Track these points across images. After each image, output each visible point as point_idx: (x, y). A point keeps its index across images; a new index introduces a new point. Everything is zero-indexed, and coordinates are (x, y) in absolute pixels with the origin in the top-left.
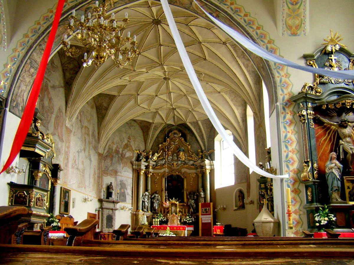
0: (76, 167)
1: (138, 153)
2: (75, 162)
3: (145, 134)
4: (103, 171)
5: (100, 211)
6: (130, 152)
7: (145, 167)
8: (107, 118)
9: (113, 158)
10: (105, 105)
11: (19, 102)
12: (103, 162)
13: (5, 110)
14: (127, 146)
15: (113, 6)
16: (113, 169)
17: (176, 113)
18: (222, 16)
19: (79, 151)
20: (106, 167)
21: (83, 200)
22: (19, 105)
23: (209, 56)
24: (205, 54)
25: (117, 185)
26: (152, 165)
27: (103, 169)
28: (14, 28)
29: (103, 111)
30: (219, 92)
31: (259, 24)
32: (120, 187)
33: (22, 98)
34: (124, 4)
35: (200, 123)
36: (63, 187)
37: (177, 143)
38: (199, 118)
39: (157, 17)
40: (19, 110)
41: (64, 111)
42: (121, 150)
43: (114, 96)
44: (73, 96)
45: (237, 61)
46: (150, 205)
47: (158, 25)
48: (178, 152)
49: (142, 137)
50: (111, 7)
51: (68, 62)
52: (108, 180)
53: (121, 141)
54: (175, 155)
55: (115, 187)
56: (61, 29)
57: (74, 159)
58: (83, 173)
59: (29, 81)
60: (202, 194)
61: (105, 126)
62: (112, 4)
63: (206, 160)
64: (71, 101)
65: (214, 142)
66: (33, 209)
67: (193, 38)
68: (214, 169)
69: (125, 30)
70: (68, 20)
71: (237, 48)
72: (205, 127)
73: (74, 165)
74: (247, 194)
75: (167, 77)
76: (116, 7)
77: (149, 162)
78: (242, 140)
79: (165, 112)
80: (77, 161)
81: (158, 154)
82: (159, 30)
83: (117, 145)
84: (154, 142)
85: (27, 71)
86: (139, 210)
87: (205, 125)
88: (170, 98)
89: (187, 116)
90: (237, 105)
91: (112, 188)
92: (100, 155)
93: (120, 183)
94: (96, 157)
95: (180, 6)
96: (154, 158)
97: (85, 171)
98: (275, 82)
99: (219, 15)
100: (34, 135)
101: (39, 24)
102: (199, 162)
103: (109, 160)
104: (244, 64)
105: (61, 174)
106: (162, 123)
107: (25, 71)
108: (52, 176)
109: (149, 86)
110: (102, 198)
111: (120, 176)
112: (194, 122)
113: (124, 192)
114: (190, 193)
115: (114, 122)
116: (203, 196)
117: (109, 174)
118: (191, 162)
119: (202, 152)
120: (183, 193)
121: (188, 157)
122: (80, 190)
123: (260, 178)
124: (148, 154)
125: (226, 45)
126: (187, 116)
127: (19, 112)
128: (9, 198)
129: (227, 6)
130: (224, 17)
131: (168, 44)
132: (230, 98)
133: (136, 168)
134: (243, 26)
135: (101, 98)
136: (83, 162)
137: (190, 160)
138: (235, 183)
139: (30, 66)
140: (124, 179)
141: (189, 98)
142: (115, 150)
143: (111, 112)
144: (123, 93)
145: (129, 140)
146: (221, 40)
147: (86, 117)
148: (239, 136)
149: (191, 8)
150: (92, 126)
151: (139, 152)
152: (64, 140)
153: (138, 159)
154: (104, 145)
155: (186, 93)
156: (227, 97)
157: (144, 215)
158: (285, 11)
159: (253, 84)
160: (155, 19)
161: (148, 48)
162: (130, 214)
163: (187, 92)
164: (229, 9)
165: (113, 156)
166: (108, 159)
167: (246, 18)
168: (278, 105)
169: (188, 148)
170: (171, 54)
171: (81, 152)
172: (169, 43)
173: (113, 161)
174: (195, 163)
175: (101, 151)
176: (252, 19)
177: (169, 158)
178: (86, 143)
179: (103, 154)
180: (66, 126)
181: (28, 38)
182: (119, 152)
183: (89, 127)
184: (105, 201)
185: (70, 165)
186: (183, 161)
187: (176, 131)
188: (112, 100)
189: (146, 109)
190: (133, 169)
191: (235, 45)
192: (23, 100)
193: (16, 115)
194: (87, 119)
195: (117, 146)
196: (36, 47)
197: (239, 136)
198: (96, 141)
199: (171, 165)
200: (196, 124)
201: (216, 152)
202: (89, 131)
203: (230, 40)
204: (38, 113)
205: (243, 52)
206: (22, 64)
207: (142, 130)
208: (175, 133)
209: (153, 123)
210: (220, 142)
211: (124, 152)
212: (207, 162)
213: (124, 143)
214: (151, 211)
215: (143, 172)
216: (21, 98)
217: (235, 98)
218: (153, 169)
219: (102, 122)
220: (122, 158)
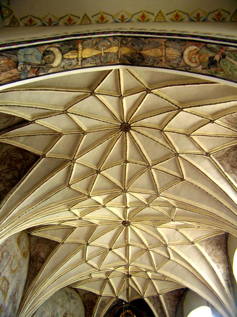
3: (88, 313)
10: (42, 255)
15: (80, 63)
17: (131, 283)
23: (187, 175)
29: (38, 264)
34: (94, 65)
35: (161, 297)
38: (160, 291)
39: (126, 120)
43: (57, 243)
47: (126, 133)
50: (78, 63)
51: (7, 170)
61: (36, 287)
62: (80, 60)
69: (86, 134)
72: (169, 305)
75: (127, 220)
76: (83, 66)
79: (118, 280)
88: (127, 254)
89: (144, 288)
90: (217, 261)
95: (166, 66)
106: (112, 297)
109: (103, 233)
115: (49, 281)
131: (136, 161)
135: (40, 244)
141: (151, 253)
143: (48, 266)
144: (68, 240)
147: (10, 262)
149: (182, 64)
155: (148, 247)
156: (202, 249)
161: (111, 165)
163: (149, 245)
183: (10, 281)
187: (130, 311)
188: (53, 249)
189: (94, 269)
194: (11, 266)
198: (15, 310)
200: (156, 299)
202: (8, 288)
207: (85, 307)
209: (101, 296)
217: (213, 251)
219: (32, 280)
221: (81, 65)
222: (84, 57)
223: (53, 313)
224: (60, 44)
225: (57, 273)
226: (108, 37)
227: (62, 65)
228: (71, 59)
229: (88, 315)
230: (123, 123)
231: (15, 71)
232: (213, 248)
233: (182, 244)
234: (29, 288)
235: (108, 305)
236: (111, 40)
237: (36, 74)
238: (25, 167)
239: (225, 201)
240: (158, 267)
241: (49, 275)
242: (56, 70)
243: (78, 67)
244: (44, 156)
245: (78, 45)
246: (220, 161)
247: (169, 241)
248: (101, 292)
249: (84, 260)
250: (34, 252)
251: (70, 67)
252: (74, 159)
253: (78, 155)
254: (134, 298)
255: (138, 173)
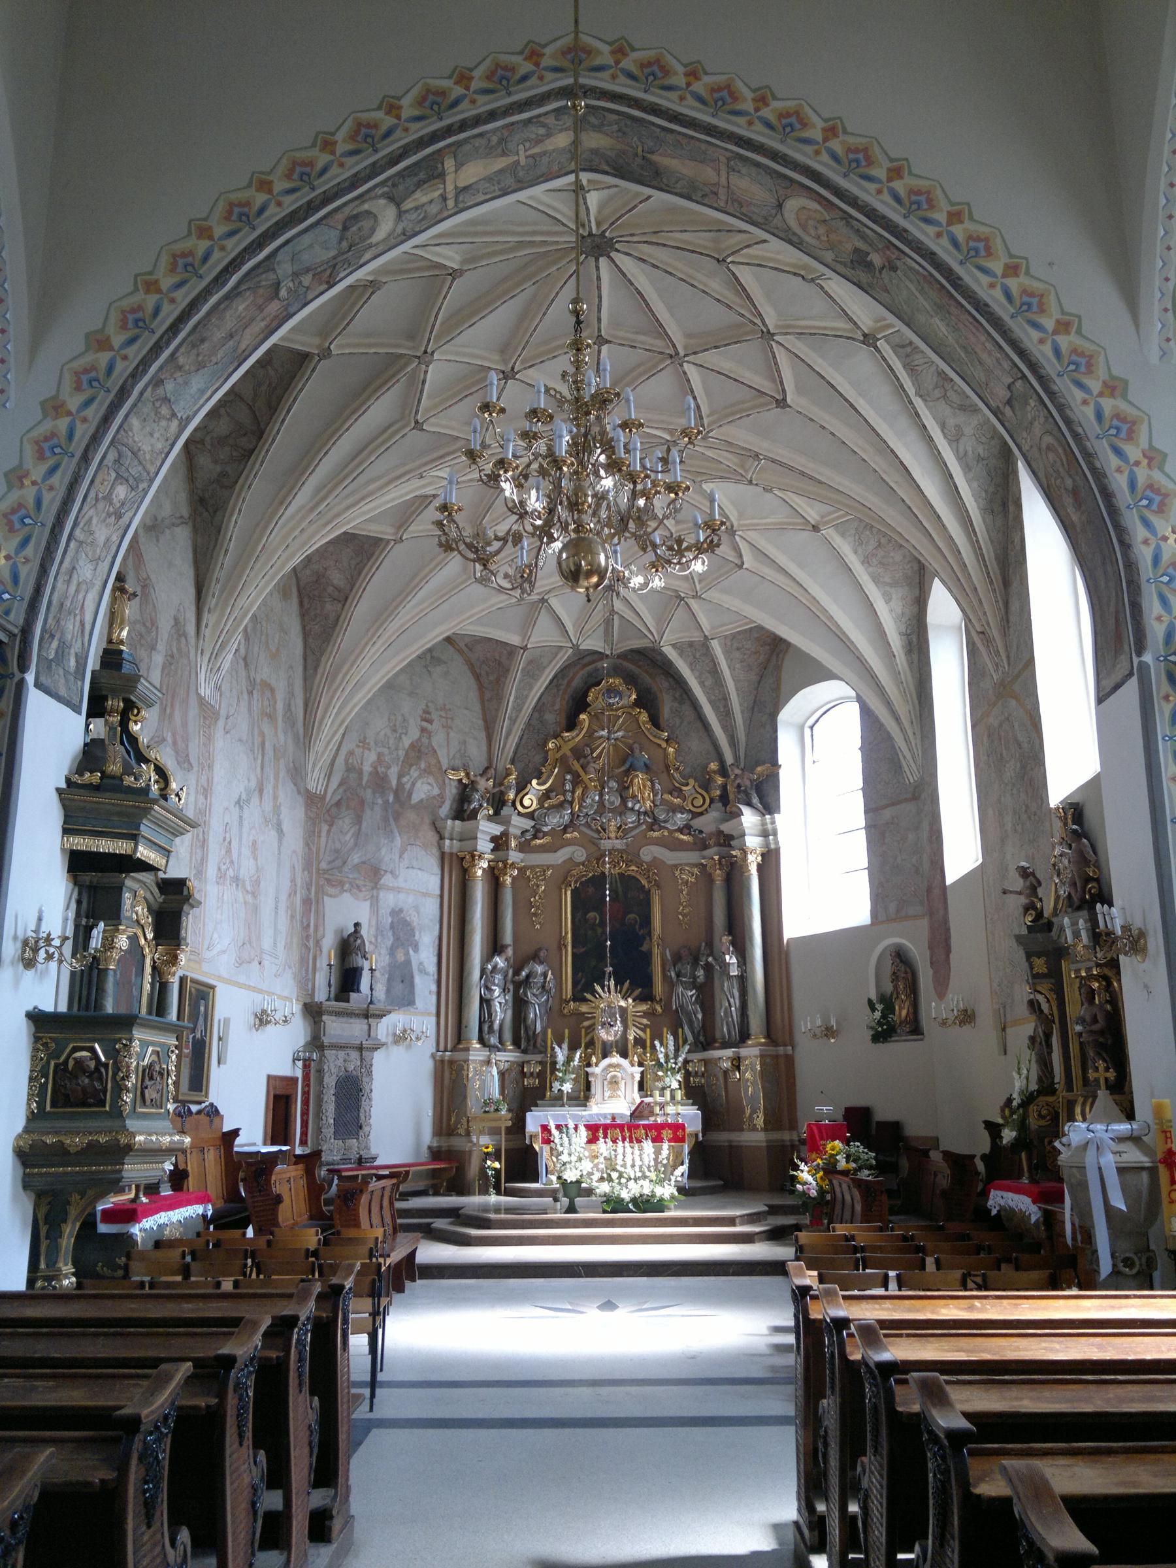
0: (231, 873)
1: (460, 781)
2: (229, 851)
4: (326, 871)
5: (310, 1059)
6: (431, 780)
7: (492, 845)
8: (346, 638)
9: (363, 811)
10: (337, 578)
11: (69, 637)
12: (324, 834)
13: (21, 684)
14: (417, 753)
15: (451, 203)
16: (364, 859)
17: (618, 605)
18: (911, 269)
19: (244, 797)
20: (337, 851)
21: (252, 1019)
22: (67, 650)
23: (799, 390)
24: (782, 383)
25: (379, 931)
26: (518, 832)
27: (324, 865)
28: (47, 305)
29: (328, 607)
30: (815, 528)
31: (1067, 309)
32: (389, 943)
33: (78, 618)
35: (716, 647)
36: (190, 975)
37: (620, 734)
38: (713, 628)
39: (598, 224)
40: (66, 672)
41: (191, 629)
42: (393, 772)
44: (226, 560)
45: (918, 415)
46: (509, 1013)
47: (597, 260)
48: (627, 772)
49: (477, 708)
52: (346, 910)
53: (395, 731)
54: (613, 784)
55: (371, 942)
56: (241, 308)
57: (225, 839)
58: (254, 895)
59: (107, 540)
60: (731, 959)
62: (451, 195)
63: (746, 810)
64: (218, 580)
65: (776, 731)
66: (131, 1124)
67: (743, 316)
68: (777, 850)
70: (274, 270)
71: (918, 360)
73: (223, 868)
74: (931, 972)
77: (506, 822)
78: (903, 730)
80: (234, 844)
81: (545, 783)
82: (599, 279)
83: (379, 750)
84: (523, 731)
85: (104, 498)
86: (469, 1040)
87: (737, 654)
89: (663, 620)
90: (887, 579)
91: (359, 948)
92: (312, 800)
93: (390, 920)
94: (300, 813)
96: (526, 802)
97: (262, 883)
98: (1131, 566)
99: (898, 263)
100: (129, 780)
101: (151, 286)
102: (708, 823)
103: (347, 820)
104: (943, 427)
105: (191, 925)
107: (97, 500)
108: (155, 938)
110: (321, 995)
111: (392, 889)
112: (691, 644)
113: (408, 963)
114: (677, 958)
115: (373, 652)
116: (734, 972)
117: (347, 886)
118: (680, 818)
119: (723, 772)
120: (648, 956)
121: (667, 797)
122: (242, 979)
123: (1024, 931)
124: (501, 784)
125: (876, 348)
126: (663, 620)
127: (67, 680)
128: (31, 1079)
129: (937, 229)
130: (918, 272)
131: (630, 336)
132: (860, 550)
133: (455, 851)
134: (1000, 319)
136: (254, 843)
137: (674, 809)
138: (874, 913)
139: (114, 475)
140: (405, 901)
142: (371, 774)
143: (362, 609)
145: (425, 724)
146: (855, 324)
148: (888, 704)
149: (778, 221)
150: (284, 678)
151: (468, 775)
152: (192, 761)
153: (463, 811)
154: (327, 757)
156: (845, 547)
157: (488, 1062)
158: (1172, 252)
159: (977, 511)
160: (590, 234)
162: (429, 1065)
164: (945, 241)
165: (362, 802)
166: (342, 813)
167: (1013, 284)
168: (1148, 666)
169: (666, 755)
170: (641, 374)
171: (248, 801)
172: (637, 333)
173: (364, 824)
174: (697, 823)
175: (315, 783)
176: (983, 230)
177: (588, 801)
178: (266, 759)
179: (323, 797)
180: (198, 694)
181: (110, 354)
182: (389, 782)
183: (273, 682)
184: (331, 1013)
185: (211, 871)
186: (645, 813)
190: (443, 855)
191: (911, 343)
192: (82, 624)
193: (59, 699)
195: (379, 755)
196: (141, 394)
197: (888, 704)
199: (599, 832)
200: (699, 651)
201: (783, 774)
203: (890, 326)
204: (142, 680)
205: (941, 374)
206: (87, 469)
207: (477, 677)
208: (611, 691)
209: (525, 648)
210: (801, 729)
211: (405, 780)
212: (749, 819)
213: (406, 742)
214: (516, 1043)
215: (485, 865)
216: (75, 615)
218: (520, 851)
220: (397, 806)
221: (456, 205)
222: (461, 185)
223: (392, 717)
224: (390, 183)
225: (394, 626)
226: (539, 116)
227: (399, 230)
228: (423, 205)
229: (490, 700)
230: (586, 234)
231: (274, 307)
232: (879, 541)
233: (781, 528)
234: (319, 676)
235: (547, 671)
236: (550, 120)
237: (328, 282)
238: (264, 388)
239: (752, 945)
240: (703, 584)
241: (370, 633)
242: (381, 248)
243: (446, 214)
244: (326, 353)
245: (443, 164)
246: (907, 356)
247: (741, 515)
248: (525, 635)
249: (469, 578)
250: (308, 572)
251: (425, 224)
252: (425, 352)
253: (438, 338)
254: (628, 642)
255: (642, 369)
